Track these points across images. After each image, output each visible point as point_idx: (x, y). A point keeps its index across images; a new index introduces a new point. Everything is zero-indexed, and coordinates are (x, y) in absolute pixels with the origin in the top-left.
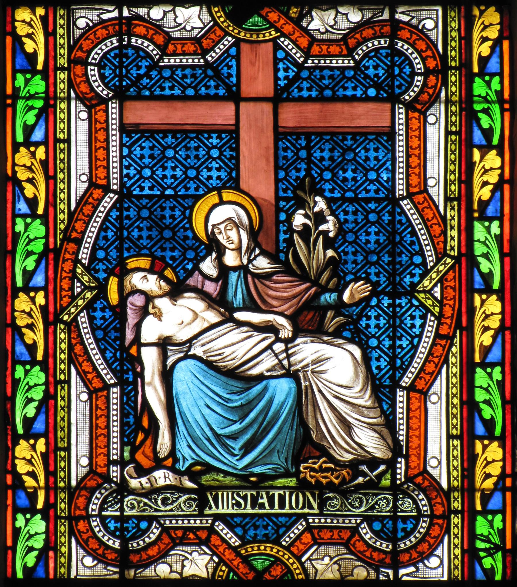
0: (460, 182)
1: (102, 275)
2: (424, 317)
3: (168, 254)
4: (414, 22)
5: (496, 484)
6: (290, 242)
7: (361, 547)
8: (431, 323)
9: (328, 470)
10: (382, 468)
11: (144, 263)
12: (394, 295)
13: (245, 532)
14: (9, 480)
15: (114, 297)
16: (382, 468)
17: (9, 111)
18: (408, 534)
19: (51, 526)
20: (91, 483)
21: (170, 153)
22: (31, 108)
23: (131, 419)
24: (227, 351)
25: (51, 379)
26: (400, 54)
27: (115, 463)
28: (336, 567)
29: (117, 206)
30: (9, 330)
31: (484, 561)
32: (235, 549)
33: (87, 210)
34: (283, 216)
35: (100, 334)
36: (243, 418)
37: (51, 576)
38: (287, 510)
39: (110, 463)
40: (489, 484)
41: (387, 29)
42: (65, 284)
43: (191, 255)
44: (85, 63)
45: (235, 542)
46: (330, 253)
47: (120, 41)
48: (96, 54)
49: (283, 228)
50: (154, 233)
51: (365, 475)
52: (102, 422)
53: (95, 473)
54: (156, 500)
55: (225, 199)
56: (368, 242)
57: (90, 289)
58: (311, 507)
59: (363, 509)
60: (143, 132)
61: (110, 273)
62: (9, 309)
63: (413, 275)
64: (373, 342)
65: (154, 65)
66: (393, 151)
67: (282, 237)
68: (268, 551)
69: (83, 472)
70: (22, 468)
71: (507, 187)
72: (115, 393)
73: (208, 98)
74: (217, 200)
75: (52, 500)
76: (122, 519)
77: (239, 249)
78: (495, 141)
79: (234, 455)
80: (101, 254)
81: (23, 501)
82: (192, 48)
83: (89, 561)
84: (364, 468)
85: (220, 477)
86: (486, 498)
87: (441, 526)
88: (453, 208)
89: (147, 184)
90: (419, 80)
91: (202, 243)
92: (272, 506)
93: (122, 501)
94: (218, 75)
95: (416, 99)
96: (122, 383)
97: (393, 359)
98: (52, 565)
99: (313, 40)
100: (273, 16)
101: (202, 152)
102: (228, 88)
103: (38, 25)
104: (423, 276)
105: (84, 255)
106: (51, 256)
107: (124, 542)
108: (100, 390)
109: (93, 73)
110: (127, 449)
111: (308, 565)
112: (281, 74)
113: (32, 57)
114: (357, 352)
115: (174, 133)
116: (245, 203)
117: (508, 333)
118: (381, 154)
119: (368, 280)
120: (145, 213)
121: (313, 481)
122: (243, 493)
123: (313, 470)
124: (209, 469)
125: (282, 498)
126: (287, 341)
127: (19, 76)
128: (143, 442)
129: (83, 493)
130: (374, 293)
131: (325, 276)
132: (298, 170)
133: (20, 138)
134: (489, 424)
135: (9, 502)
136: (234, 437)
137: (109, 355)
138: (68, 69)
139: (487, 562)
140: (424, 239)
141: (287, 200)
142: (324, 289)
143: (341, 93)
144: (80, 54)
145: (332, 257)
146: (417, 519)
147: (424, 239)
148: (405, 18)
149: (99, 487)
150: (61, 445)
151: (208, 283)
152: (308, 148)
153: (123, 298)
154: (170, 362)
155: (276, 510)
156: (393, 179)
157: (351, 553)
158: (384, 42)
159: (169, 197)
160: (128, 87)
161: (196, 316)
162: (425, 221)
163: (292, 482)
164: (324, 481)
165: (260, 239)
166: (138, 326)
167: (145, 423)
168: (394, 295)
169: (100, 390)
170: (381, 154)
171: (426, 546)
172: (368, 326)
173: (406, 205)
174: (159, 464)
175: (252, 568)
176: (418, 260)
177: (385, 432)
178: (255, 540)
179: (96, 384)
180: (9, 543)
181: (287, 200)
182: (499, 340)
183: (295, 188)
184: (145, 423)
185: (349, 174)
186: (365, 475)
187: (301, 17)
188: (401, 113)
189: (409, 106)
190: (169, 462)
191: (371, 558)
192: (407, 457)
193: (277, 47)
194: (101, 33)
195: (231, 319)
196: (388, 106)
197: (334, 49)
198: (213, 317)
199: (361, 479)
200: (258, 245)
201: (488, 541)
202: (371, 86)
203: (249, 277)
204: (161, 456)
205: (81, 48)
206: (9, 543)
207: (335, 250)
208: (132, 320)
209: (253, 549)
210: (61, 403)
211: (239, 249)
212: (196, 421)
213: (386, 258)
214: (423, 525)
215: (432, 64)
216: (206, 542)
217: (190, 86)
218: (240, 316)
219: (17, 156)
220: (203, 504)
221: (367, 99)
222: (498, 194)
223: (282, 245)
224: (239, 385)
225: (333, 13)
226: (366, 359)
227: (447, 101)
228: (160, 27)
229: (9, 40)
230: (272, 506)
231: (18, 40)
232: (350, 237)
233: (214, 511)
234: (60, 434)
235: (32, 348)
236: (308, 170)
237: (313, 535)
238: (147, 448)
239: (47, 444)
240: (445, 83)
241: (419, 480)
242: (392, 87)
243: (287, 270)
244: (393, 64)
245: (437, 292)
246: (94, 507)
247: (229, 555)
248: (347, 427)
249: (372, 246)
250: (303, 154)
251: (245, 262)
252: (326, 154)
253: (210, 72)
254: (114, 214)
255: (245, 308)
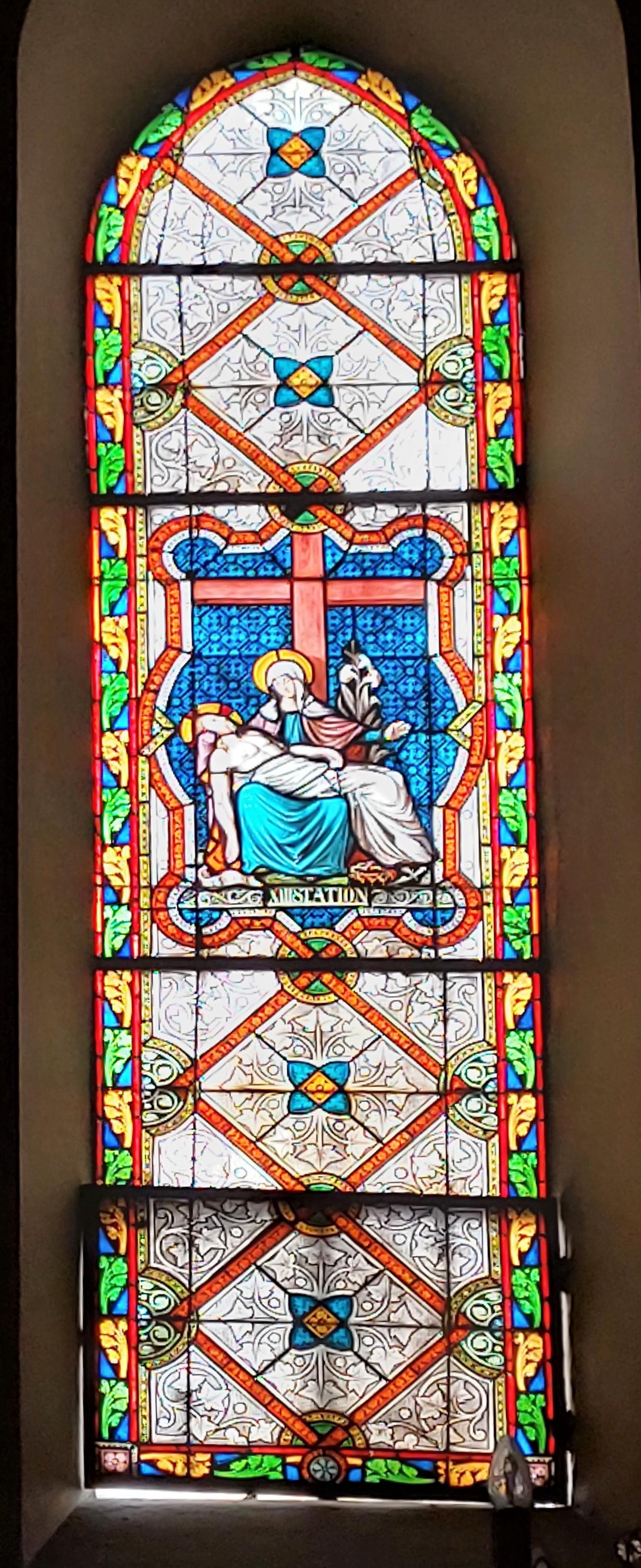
0: (486, 643)
1: (177, 719)
2: (456, 749)
3: (234, 702)
4: (443, 516)
5: (523, 883)
6: (338, 691)
7: (405, 931)
8: (463, 754)
9: (375, 871)
10: (422, 869)
11: (215, 708)
12: (430, 732)
13: (304, 920)
14: (99, 881)
15: (187, 737)
16: (422, 869)
17: (96, 589)
18: (445, 922)
19: (136, 917)
20: (170, 883)
21: (234, 621)
22: (114, 587)
23: (204, 832)
24: (285, 778)
25: (134, 800)
26: (431, 541)
27: (191, 866)
28: (384, 948)
29: (191, 663)
30: (98, 762)
31: (514, 943)
32: (295, 934)
33: (163, 667)
34: (332, 671)
35: (176, 764)
36: (301, 830)
37: (136, 954)
38: (340, 903)
39: (185, 866)
40: (517, 883)
41: (420, 521)
42: (146, 725)
43: (253, 701)
44: (160, 551)
45: (296, 928)
46: (374, 700)
47: (191, 533)
48: (171, 543)
49: (332, 680)
50: (222, 685)
51: (408, 875)
52: (450, 834)
53: (173, 874)
54: (226, 897)
55: (282, 657)
56: (406, 691)
57: (168, 729)
58: (360, 900)
59: (406, 902)
60: (211, 606)
61: (184, 716)
62: (97, 747)
63: (445, 717)
64: (412, 770)
65: (220, 553)
66: (426, 618)
67: (332, 688)
68: (324, 935)
69: (162, 873)
70: (109, 870)
71: (526, 647)
72: (190, 811)
73: (266, 578)
74: (275, 659)
75: (136, 896)
76: (197, 910)
77: (294, 697)
78: (515, 609)
79: (294, 860)
80: (176, 702)
81: (110, 896)
82: (252, 538)
83: (169, 943)
84: (406, 870)
85: (282, 877)
86: (514, 893)
87: (475, 916)
88: (479, 663)
89: (215, 647)
90: (447, 563)
91: (263, 693)
92: (327, 900)
93: (196, 896)
94: (274, 560)
95: (445, 578)
96: (196, 803)
97: (430, 784)
98: (136, 945)
99: (356, 531)
100: (321, 513)
101: (262, 621)
102: (284, 569)
103: (122, 521)
104: (455, 718)
105: (162, 702)
106: (134, 703)
107: (199, 928)
108: (177, 808)
109: (168, 559)
110: (201, 855)
111: (359, 947)
112: (329, 559)
113: (115, 548)
114: (399, 777)
115: (238, 606)
116: (296, 660)
117: (530, 763)
118: (417, 621)
119: (406, 721)
120: (213, 669)
121: (363, 881)
122: (301, 890)
123: (360, 871)
124: (272, 871)
125: (335, 894)
126: (337, 769)
127: (104, 561)
128: (214, 850)
129: (162, 890)
130: (412, 731)
131: (370, 717)
132: (344, 634)
133: (106, 611)
134: (516, 836)
135: (99, 896)
136: (293, 845)
137: (183, 781)
138: (147, 556)
139: (517, 945)
140: (454, 686)
141: (336, 658)
142: (368, 729)
143: (380, 573)
144: (157, 544)
145: (376, 705)
146: (454, 909)
147: (454, 686)
148: (435, 513)
149: (177, 885)
150: (142, 851)
151: (268, 724)
152: (354, 617)
153: (195, 737)
154: (236, 788)
155: (331, 902)
156: (425, 642)
157: (396, 936)
158: (417, 532)
159: (234, 657)
160: (198, 570)
161: (259, 750)
162: (456, 675)
163: (345, 881)
164: (372, 881)
165: (313, 687)
166: (208, 758)
167: (216, 834)
168: (430, 732)
169: (177, 808)
170: (417, 621)
171: (462, 931)
172: (408, 758)
173: (439, 662)
174: (228, 867)
175: (310, 949)
176: (449, 705)
177: (425, 841)
178: (312, 926)
179: (173, 804)
180: (99, 929)
181: (336, 658)
182: (523, 767)
183: (343, 649)
184: (216, 834)
185: (390, 637)
186: (408, 875)
187: (345, 513)
188: (432, 587)
189: (439, 582)
190: (237, 865)
191: (415, 941)
192: (444, 861)
193: (324, 537)
194: (174, 527)
195: (287, 753)
196: (422, 583)
197: (375, 538)
198: (273, 750)
199: (404, 879)
200: (311, 693)
201: (516, 926)
202: (406, 567)
203: (305, 720)
204: (229, 861)
205: (157, 540)
206: (99, 929)
207: (378, 697)
208: (203, 753)
209: (312, 933)
210: (142, 818)
211: (294, 697)
212: (260, 834)
213: (423, 704)
214: (459, 916)
215: (459, 549)
216: (270, 928)
217: (250, 568)
218: (295, 750)
219: (103, 625)
220: (266, 898)
221: (402, 578)
222: (519, 653)
223: (332, 694)
224: (294, 804)
225: (373, 509)
226: (407, 784)
227: (473, 579)
228: (225, 523)
229: (95, 533)
230: (327, 900)
231: (102, 534)
232: (391, 687)
233: (277, 904)
234: (142, 843)
235: (117, 777)
236: (354, 635)
237: (363, 923)
238: (218, 854)
239: (132, 852)
240: (470, 563)
241: (454, 879)
242: (424, 568)
243: (337, 714)
244: (425, 549)
245: (468, 731)
246: (172, 901)
247: (289, 938)
248: (392, 838)
249: (410, 694)
250: (349, 621)
251: (300, 708)
252: (369, 622)
253: (268, 558)
254: (187, 670)
255: (300, 743)
